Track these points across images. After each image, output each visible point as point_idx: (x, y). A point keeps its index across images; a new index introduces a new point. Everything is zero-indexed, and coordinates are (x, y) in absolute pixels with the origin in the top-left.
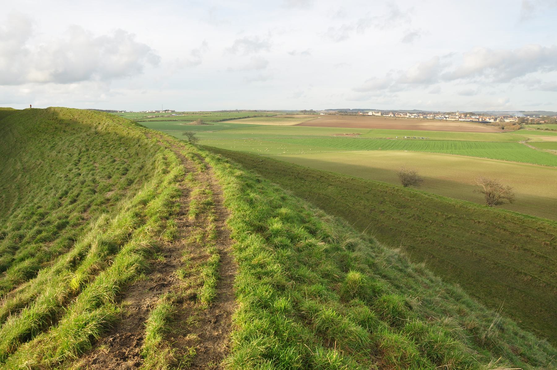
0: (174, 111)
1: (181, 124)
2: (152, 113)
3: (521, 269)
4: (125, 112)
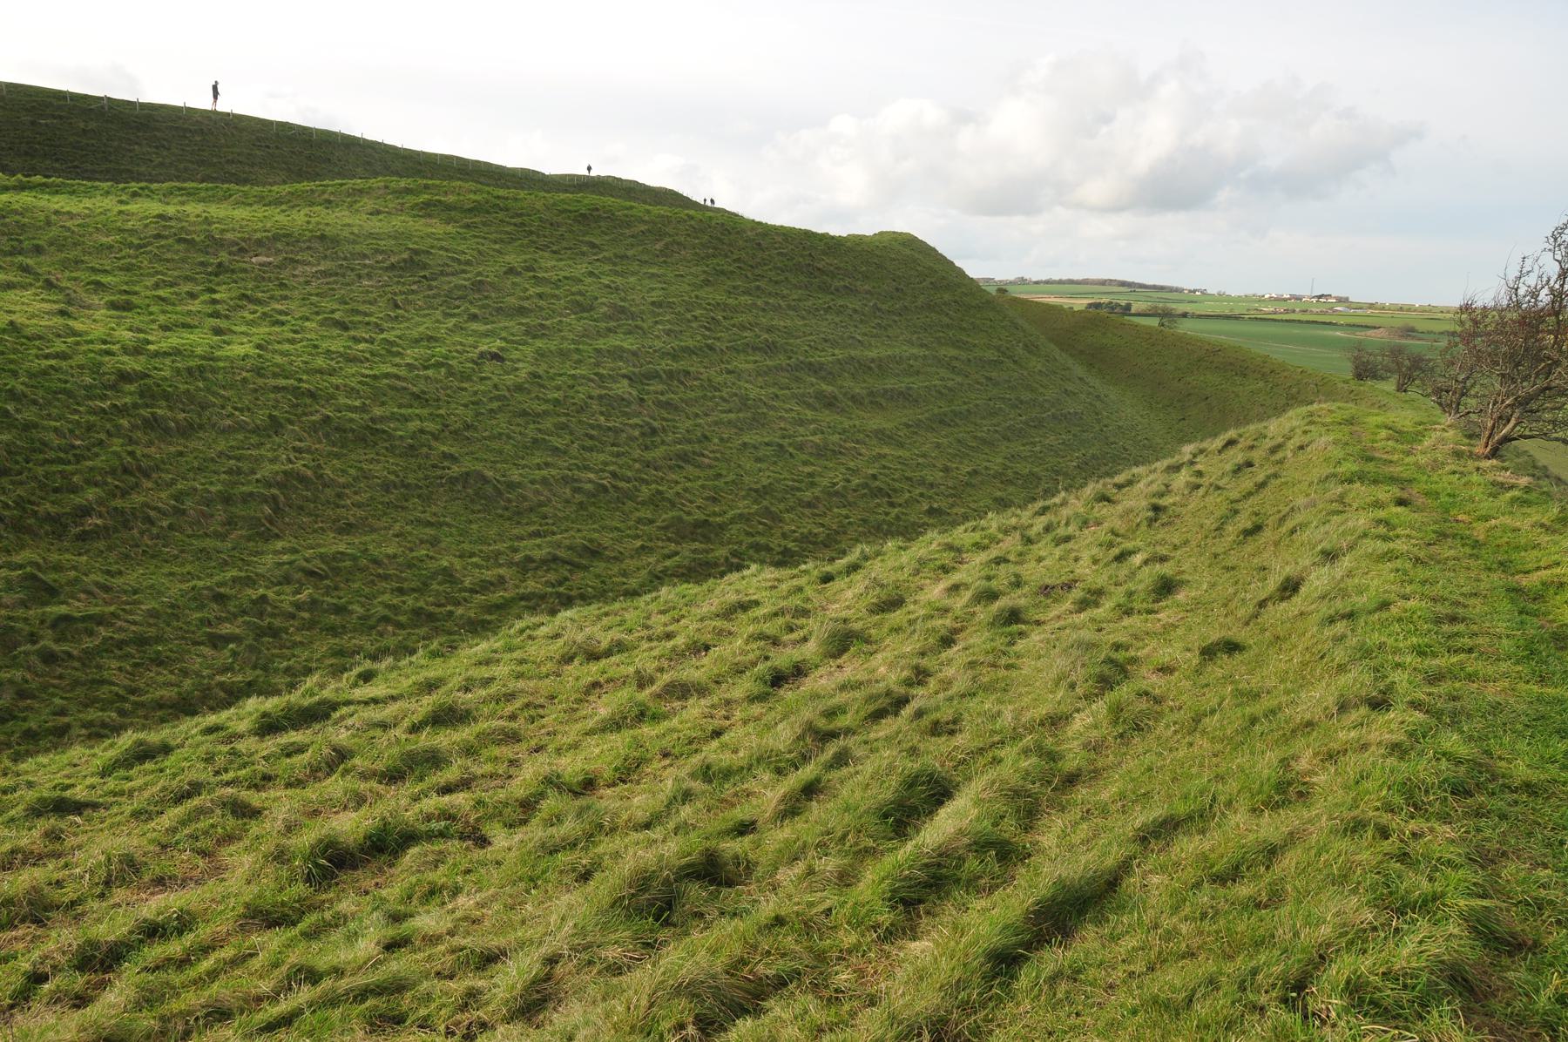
0: (1347, 299)
1: (1338, 333)
2: (1279, 299)
3: (1131, 994)
4: (1203, 292)
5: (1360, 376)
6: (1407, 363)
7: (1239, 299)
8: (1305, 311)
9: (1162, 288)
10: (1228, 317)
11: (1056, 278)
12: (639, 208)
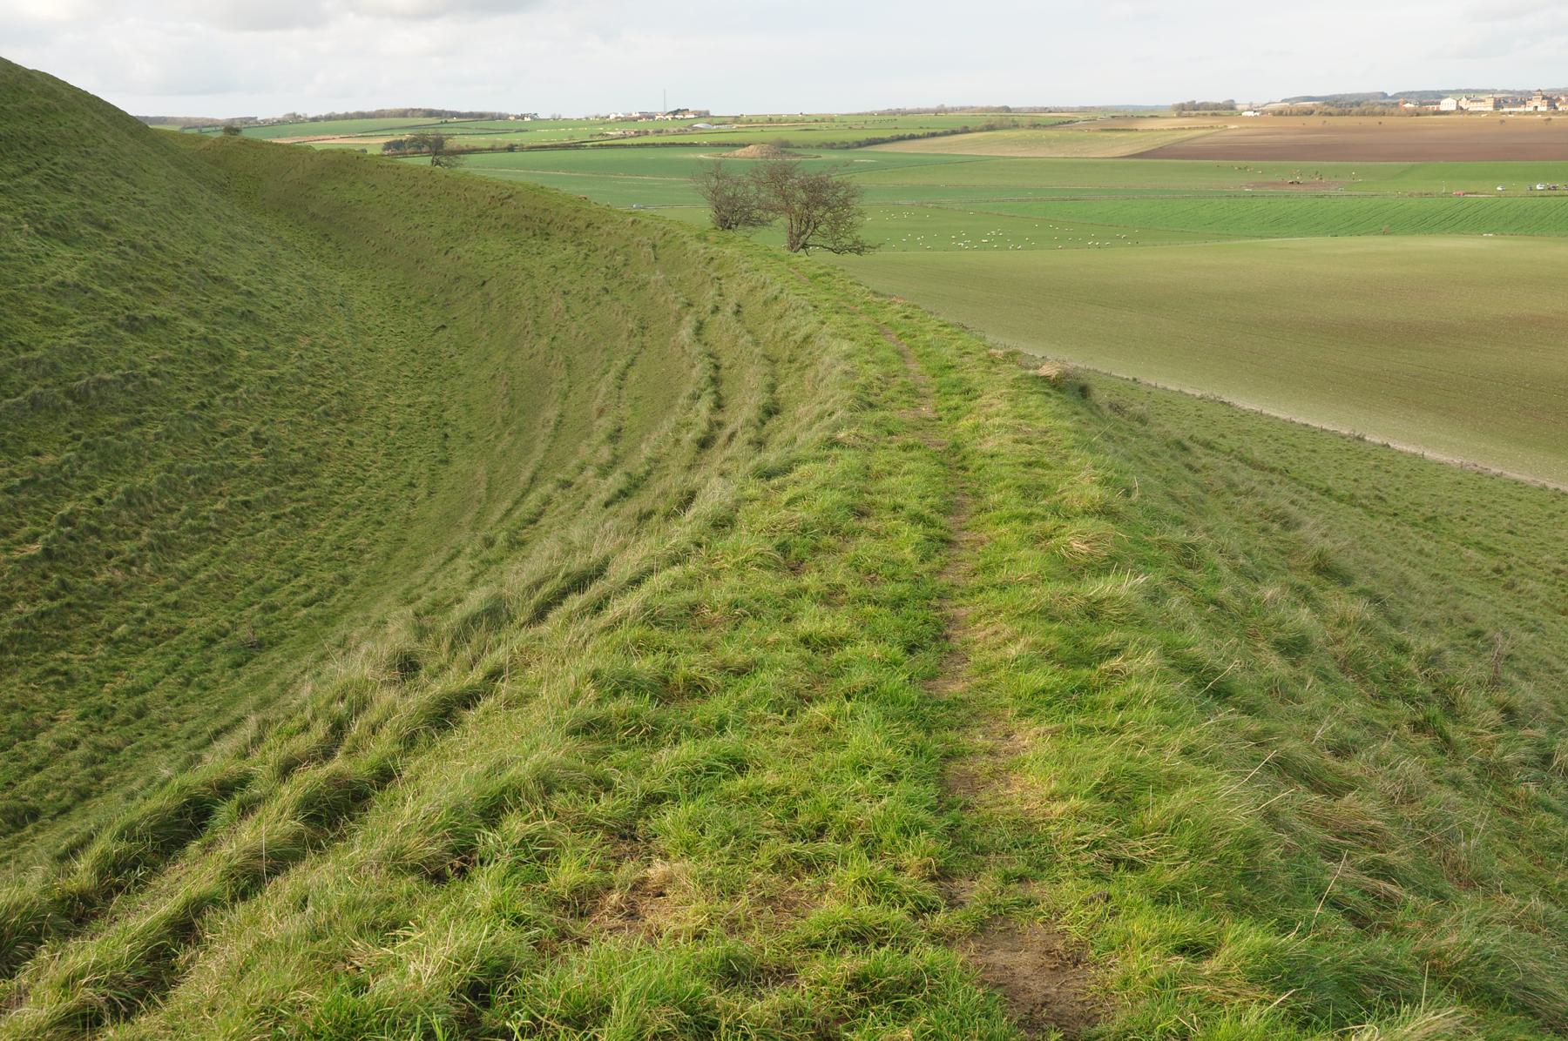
4: (534, 117)
5: (725, 223)
6: (802, 195)
7: (579, 123)
8: (659, 132)
9: (481, 116)
10: (566, 147)
11: (340, 111)
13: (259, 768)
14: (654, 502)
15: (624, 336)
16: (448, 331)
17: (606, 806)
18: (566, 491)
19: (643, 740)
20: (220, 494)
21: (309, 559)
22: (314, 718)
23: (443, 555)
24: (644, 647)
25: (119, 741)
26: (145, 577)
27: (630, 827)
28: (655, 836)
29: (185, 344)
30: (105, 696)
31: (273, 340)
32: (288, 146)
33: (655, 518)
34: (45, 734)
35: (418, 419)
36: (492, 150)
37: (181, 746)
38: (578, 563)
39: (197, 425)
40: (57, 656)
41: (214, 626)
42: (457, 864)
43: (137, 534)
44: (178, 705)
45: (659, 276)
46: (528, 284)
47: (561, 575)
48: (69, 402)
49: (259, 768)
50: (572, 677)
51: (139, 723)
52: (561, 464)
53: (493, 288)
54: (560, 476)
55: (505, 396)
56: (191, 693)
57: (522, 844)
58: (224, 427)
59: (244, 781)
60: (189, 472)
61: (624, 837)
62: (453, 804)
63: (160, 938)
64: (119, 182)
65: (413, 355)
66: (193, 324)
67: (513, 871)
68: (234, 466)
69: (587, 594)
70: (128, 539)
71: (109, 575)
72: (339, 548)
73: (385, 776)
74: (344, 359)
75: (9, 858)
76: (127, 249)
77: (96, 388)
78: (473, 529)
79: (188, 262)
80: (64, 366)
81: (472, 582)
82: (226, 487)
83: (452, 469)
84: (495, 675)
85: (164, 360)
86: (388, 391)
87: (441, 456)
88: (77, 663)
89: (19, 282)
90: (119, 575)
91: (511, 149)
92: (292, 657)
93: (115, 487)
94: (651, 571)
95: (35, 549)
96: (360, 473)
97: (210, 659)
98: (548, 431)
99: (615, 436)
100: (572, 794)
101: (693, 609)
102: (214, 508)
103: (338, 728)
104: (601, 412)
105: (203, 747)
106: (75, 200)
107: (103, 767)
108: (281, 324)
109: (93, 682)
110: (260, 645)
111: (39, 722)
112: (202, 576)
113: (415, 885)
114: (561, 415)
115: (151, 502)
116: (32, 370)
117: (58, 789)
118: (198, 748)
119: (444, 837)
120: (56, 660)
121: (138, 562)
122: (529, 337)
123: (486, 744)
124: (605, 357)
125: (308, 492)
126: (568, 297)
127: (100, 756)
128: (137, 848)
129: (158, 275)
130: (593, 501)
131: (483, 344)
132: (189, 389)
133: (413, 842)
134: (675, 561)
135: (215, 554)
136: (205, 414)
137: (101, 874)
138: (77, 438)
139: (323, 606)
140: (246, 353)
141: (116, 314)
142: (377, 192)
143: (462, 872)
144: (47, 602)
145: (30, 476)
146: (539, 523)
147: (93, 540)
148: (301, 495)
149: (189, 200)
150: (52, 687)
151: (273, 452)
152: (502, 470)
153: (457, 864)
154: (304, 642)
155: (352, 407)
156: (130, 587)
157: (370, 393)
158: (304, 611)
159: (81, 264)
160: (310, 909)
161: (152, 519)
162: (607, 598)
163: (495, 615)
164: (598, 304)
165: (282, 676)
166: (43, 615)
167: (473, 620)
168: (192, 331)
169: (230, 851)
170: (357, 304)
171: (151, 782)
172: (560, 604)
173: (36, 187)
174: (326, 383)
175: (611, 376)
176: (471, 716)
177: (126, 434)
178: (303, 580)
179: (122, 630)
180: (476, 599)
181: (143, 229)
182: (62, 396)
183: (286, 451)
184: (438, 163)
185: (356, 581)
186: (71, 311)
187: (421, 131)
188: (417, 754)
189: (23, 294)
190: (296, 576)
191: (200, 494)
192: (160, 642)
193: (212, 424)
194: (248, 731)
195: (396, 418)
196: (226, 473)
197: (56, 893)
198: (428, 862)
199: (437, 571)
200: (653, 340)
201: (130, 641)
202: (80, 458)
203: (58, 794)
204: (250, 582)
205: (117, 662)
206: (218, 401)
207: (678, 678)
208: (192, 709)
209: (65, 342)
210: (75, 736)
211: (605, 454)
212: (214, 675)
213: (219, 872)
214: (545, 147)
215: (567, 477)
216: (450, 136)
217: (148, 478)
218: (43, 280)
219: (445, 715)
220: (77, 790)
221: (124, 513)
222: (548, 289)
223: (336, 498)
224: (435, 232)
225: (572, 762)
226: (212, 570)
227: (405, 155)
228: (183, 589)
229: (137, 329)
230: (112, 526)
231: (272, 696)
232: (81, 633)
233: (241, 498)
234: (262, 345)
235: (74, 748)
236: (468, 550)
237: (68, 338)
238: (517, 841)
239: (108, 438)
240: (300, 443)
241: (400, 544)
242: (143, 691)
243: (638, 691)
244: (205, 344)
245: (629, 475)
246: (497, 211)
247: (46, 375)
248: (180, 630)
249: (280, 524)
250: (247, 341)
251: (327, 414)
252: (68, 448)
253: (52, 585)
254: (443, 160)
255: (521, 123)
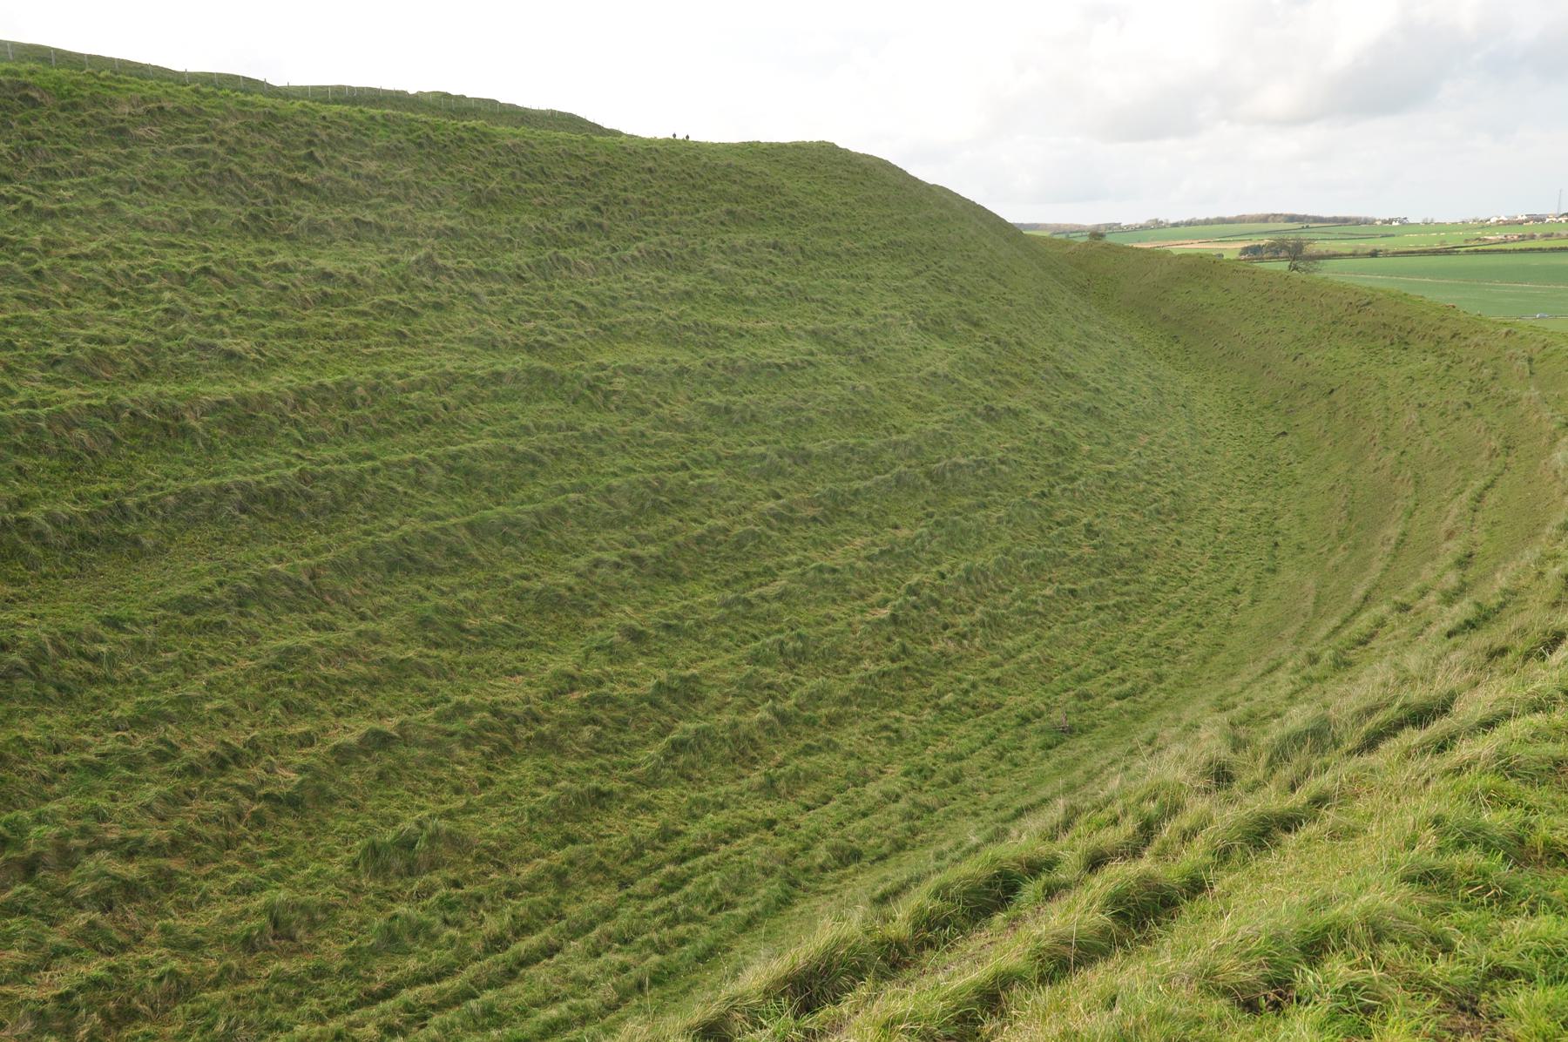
4: (1403, 222)
8: (1548, 236)
9: (1345, 221)
10: (1436, 252)
12: (259, 98)
13: (1067, 854)
14: (1507, 640)
15: (1485, 454)
16: (1288, 439)
17: (1441, 969)
18: (1402, 615)
19: (1490, 903)
20: (1050, 580)
21: (1127, 653)
22: (1125, 813)
23: (1262, 666)
24: (1496, 799)
25: (935, 802)
26: (973, 651)
27: (1471, 999)
28: (1502, 1016)
29: (1034, 435)
30: (927, 758)
31: (1115, 436)
32: (1147, 251)
33: (1510, 657)
34: (873, 784)
35: (1249, 525)
36: (1354, 255)
37: (988, 816)
38: (1418, 695)
39: (1036, 513)
40: (891, 714)
41: (1030, 706)
42: (1272, 996)
43: (971, 609)
44: (990, 777)
45: (1534, 392)
46: (1381, 394)
47: (1398, 704)
48: (928, 482)
49: (1067, 854)
50: (1411, 819)
51: (954, 788)
52: (1399, 586)
53: (1340, 398)
54: (1397, 598)
55: (1344, 509)
56: (1003, 766)
57: (1345, 990)
58: (1060, 516)
59: (1051, 864)
60: (1024, 556)
61: (1463, 1009)
62: (1273, 932)
63: (969, 1003)
64: (992, 283)
65: (1250, 460)
66: (1043, 416)
67: (1333, 1018)
68: (1065, 555)
69: (1430, 728)
70: (963, 613)
71: (943, 645)
72: (1156, 645)
73: (1196, 887)
74: (1180, 460)
75: (833, 891)
76: (992, 344)
77: (951, 471)
78: (1296, 643)
79: (1044, 359)
80: (926, 448)
81: (1292, 697)
82: (1057, 573)
83: (1279, 579)
84: (1319, 801)
85: (1013, 449)
86: (1221, 494)
87: (1269, 564)
88: (908, 725)
89: (898, 371)
90: (952, 646)
91: (1374, 254)
92: (1099, 748)
93: (957, 564)
94: (1508, 716)
95: (884, 613)
96: (1184, 574)
97: (1024, 737)
98: (1387, 549)
99: (1464, 562)
100: (1405, 947)
101: (1558, 765)
102: (1043, 592)
103: (1148, 829)
104: (1450, 535)
105: (1009, 821)
106: (954, 299)
107: (919, 823)
108: (1124, 421)
109: (918, 742)
110: (1070, 731)
111: (870, 772)
112: (1024, 656)
113: (1227, 1010)
114: (1404, 534)
115: (986, 581)
116: (900, 451)
117: (879, 836)
118: (1004, 821)
119: (1260, 965)
120: (889, 717)
121: (969, 636)
122: (1376, 449)
123: (1305, 873)
124: (1460, 475)
125: (1133, 587)
126: (1424, 411)
127: (917, 812)
128: (949, 909)
129: (1017, 369)
130: (1434, 629)
131: (1325, 453)
132: (1032, 478)
133: (1227, 963)
134: (1536, 708)
135: (1038, 637)
136: (1045, 502)
137: (916, 926)
138: (930, 515)
139: (1135, 701)
140: (1087, 447)
141: (976, 403)
142: (1230, 296)
143: (1276, 1005)
144: (889, 663)
145: (888, 547)
146: (1369, 646)
147: (933, 610)
148: (1125, 589)
149: (1052, 300)
150: (884, 742)
151: (1103, 545)
152: (1333, 585)
153: (1272, 996)
154: (1113, 734)
155: (1184, 507)
156: (960, 658)
157: (1202, 496)
158: (1117, 704)
159: (952, 358)
160: (1118, 1010)
161: (986, 597)
162: (1453, 738)
163: (1319, 736)
164: (1458, 419)
165: (1089, 764)
166: (884, 674)
167: (1298, 739)
168: (1041, 424)
169: (1039, 932)
170: (1199, 405)
171: (959, 845)
172: (1395, 736)
173: (924, 287)
174: (1161, 482)
175: (1466, 497)
176: (1291, 840)
177: (973, 515)
178: (1118, 673)
179: (949, 698)
180: (1299, 717)
181: (1008, 327)
182: (922, 476)
183: (1115, 545)
184: (1296, 268)
185: (1171, 680)
186: (938, 399)
187: (1281, 236)
188: (1230, 870)
189: (901, 382)
190: (1112, 668)
191: (1031, 578)
192: (981, 714)
193: (1049, 512)
194: (1056, 812)
195: (1229, 523)
196: (1057, 560)
197: (877, 935)
198: (1242, 987)
199: (1254, 681)
200: (1519, 462)
201: (954, 710)
202: (931, 534)
203: (878, 841)
204: (1068, 669)
205: (940, 727)
206: (1057, 491)
207: (1537, 839)
208: (1003, 782)
209: (930, 427)
210: (898, 790)
211: (1452, 579)
212: (1025, 753)
213: (1027, 950)
214: (1413, 252)
215: (1406, 600)
216: (1311, 241)
217: (987, 558)
218: (919, 370)
219: (1263, 835)
220: (895, 841)
221: (962, 589)
222: (1402, 401)
223: (1159, 596)
224: (1286, 338)
225: (1405, 911)
226: (1035, 652)
227: (1262, 260)
228: (1006, 667)
229: (993, 418)
230: (951, 600)
231: (1078, 782)
232: (914, 695)
233: (1068, 586)
234: (1104, 440)
235: (896, 801)
236: (1290, 664)
237: (933, 424)
238: (1340, 986)
239: (956, 518)
240: (1130, 539)
241: (1217, 648)
242: (961, 758)
243: (1488, 847)
244: (1051, 436)
245: (1478, 605)
246: (1353, 318)
247: (911, 456)
248: (998, 706)
249: (1102, 615)
250: (1090, 435)
251: (1159, 513)
252: (922, 523)
253: (894, 648)
254: (1301, 265)
255: (1388, 227)
